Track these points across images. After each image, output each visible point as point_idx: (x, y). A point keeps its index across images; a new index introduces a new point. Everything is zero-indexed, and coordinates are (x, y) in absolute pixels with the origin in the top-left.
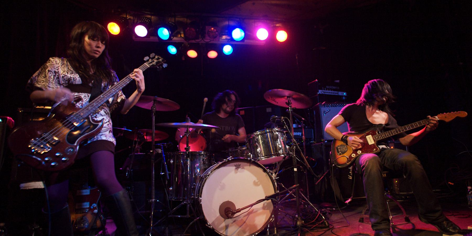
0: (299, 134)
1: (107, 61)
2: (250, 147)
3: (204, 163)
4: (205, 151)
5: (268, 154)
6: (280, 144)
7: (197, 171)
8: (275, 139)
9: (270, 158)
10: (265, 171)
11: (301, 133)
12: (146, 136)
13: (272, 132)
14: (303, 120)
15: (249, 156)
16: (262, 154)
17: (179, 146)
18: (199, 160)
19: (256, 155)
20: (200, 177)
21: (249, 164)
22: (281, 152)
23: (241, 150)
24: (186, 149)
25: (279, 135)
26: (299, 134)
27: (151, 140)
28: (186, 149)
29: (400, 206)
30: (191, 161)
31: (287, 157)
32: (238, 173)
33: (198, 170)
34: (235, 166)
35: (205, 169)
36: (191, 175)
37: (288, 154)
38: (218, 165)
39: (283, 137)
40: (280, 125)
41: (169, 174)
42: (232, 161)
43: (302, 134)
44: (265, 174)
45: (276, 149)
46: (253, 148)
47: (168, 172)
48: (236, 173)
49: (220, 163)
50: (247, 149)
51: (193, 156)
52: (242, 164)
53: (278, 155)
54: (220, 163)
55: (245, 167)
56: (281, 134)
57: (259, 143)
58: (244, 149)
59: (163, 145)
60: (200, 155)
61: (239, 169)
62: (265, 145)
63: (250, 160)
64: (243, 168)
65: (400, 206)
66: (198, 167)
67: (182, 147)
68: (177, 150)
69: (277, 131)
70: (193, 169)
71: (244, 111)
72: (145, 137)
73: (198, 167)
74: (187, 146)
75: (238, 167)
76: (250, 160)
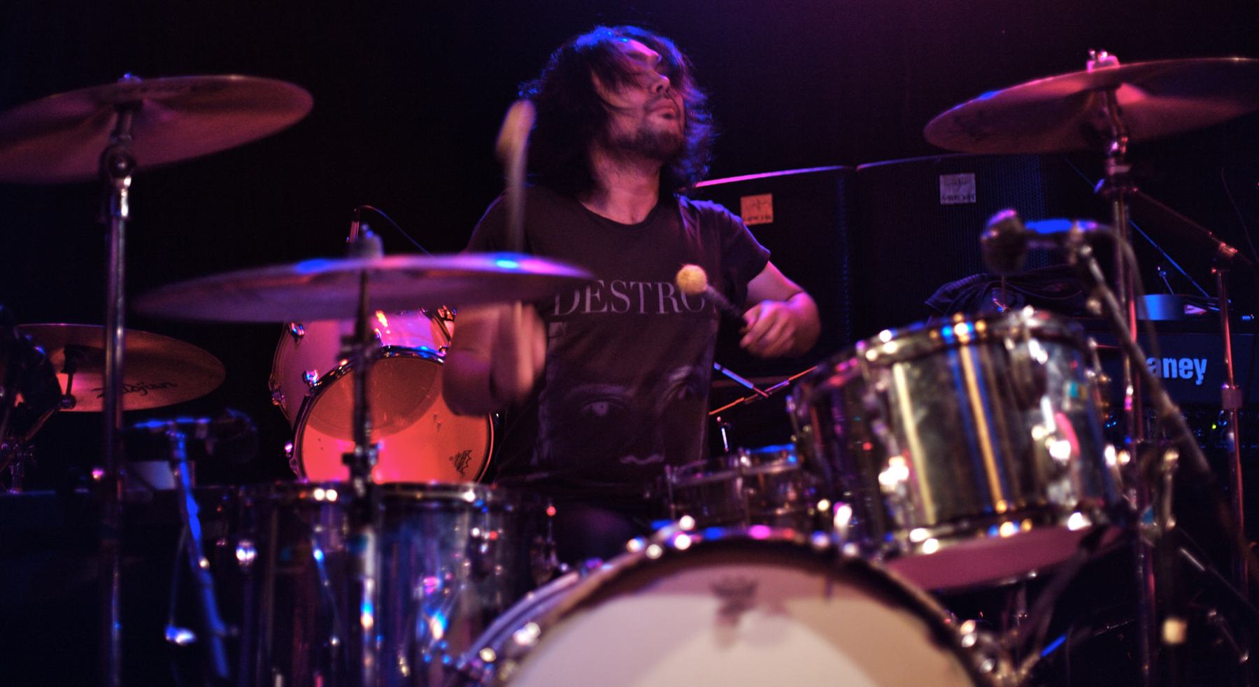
0: (1192, 368)
1: (867, 541)
2: (828, 454)
3: (479, 572)
4: (484, 479)
5: (964, 511)
6: (1052, 436)
7: (428, 633)
8: (1016, 394)
9: (980, 541)
10: (944, 638)
11: (1201, 367)
12: (70, 369)
13: (990, 342)
14: (1223, 260)
15: (824, 523)
16: (920, 509)
17: (299, 450)
18: (446, 546)
19: (877, 518)
20: (450, 669)
21: (818, 582)
22: (1062, 491)
23: (751, 481)
24: (348, 459)
25: (1053, 368)
26: (1192, 368)
27: (95, 406)
28: (348, 459)
29: (721, 476)
30: (385, 550)
31: (1108, 537)
32: (742, 653)
33: (437, 627)
34: (720, 591)
35: (486, 617)
36: (387, 660)
37: (1119, 512)
38: (592, 581)
39: (1077, 377)
40: (1057, 288)
41: (230, 643)
42: (700, 554)
43: (1216, 373)
44: (938, 661)
45: (1028, 470)
46: (848, 462)
47: (219, 628)
48: (725, 643)
49: (607, 569)
50: (808, 465)
51: (400, 513)
52: (766, 576)
53: (1047, 516)
54: (607, 569)
55: (798, 606)
56: (1068, 358)
57: (894, 424)
58: (777, 468)
59: (189, 430)
60: (453, 508)
61: (750, 621)
62: (946, 435)
63: (833, 552)
64: (778, 608)
65: (721, 476)
66: (436, 601)
67: (321, 457)
68: (286, 472)
69: (1037, 334)
70: (399, 610)
71: (768, 198)
72: (63, 379)
73: (436, 601)
74: (360, 437)
75: (735, 603)
76: (833, 552)
